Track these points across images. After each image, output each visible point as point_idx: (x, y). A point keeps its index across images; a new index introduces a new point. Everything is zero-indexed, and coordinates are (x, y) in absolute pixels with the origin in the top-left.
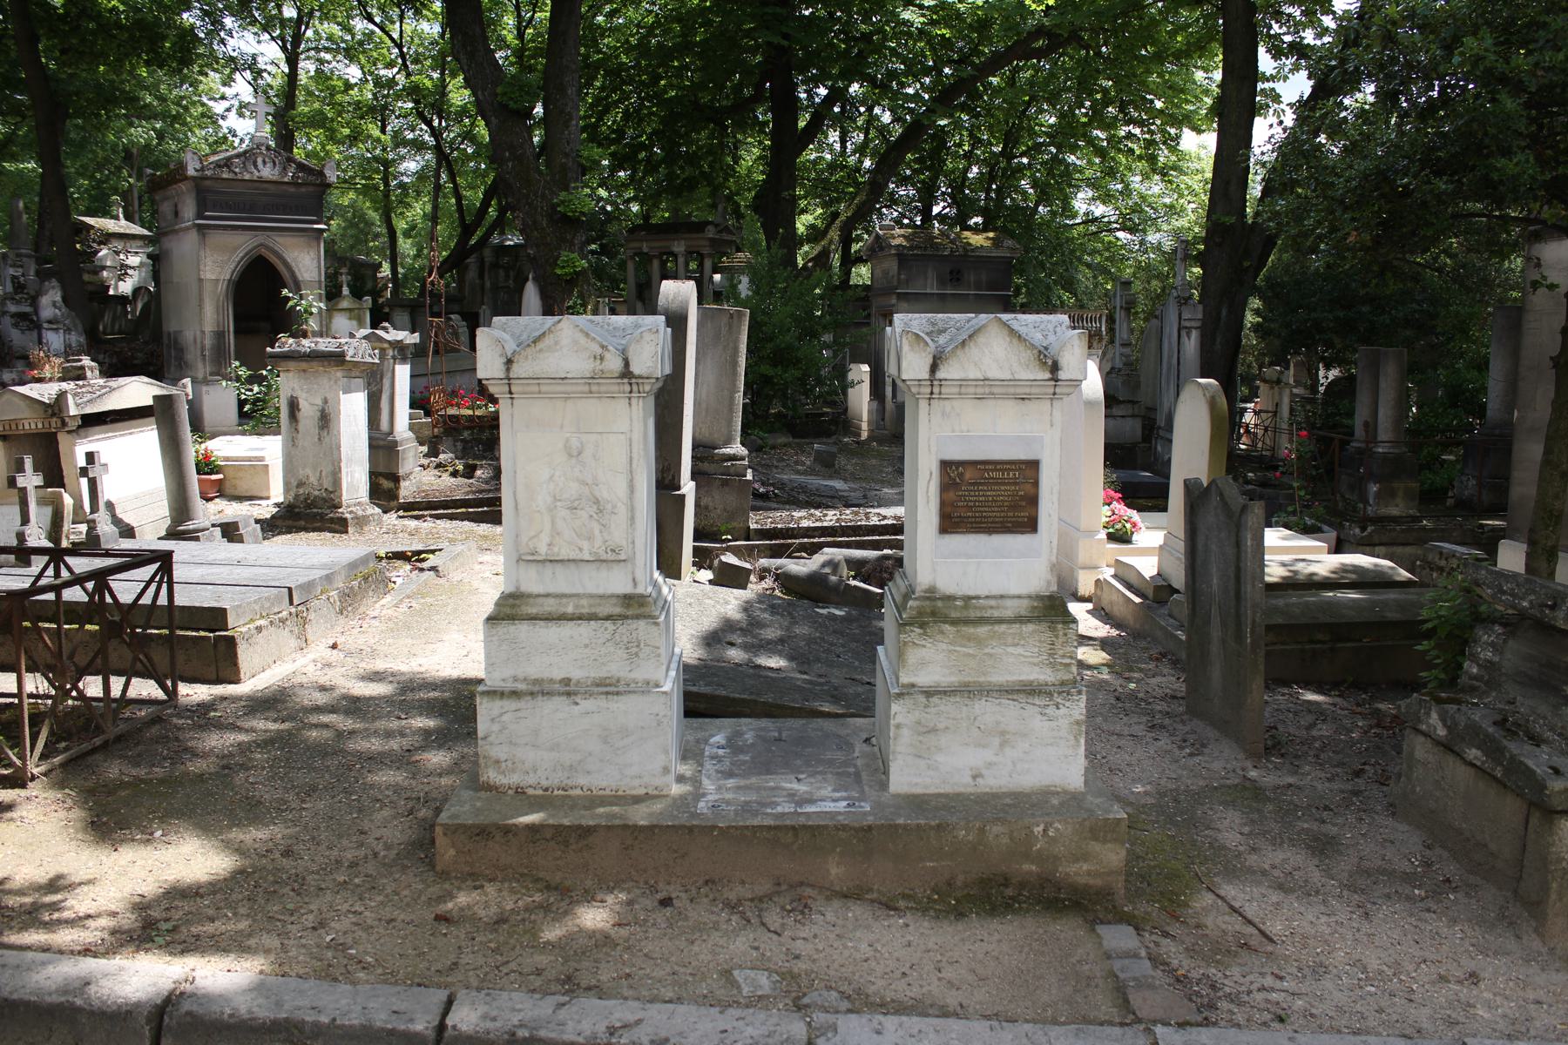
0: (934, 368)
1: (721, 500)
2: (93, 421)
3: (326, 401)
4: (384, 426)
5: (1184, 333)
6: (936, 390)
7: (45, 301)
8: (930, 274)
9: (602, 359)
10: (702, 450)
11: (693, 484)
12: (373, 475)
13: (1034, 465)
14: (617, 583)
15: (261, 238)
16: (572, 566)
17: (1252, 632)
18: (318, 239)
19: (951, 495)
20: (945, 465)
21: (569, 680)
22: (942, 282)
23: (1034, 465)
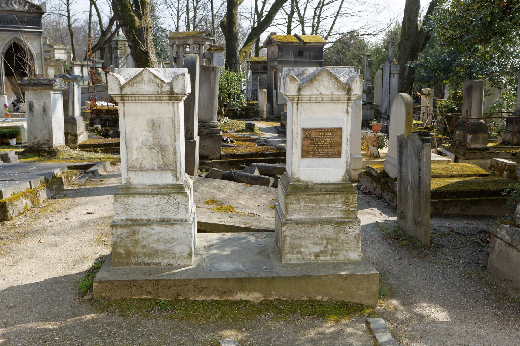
0: (299, 90)
1: (209, 143)
3: (45, 103)
4: (70, 114)
5: (392, 75)
6: (300, 99)
8: (290, 53)
9: (162, 86)
10: (202, 124)
11: (199, 137)
12: (66, 134)
14: (168, 179)
15: (15, 35)
16: (150, 172)
17: (426, 196)
18: (40, 36)
20: (304, 130)
21: (150, 219)
22: (295, 56)
23: (340, 129)
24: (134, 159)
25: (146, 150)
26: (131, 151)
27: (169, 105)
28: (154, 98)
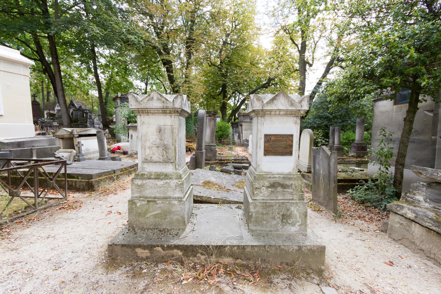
2: (80, 136)
7: (95, 119)
13: (265, 155)
16: (158, 163)
19: (267, 144)
24: (146, 154)
25: (154, 149)
26: (145, 149)
27: (171, 117)
28: (161, 111)
